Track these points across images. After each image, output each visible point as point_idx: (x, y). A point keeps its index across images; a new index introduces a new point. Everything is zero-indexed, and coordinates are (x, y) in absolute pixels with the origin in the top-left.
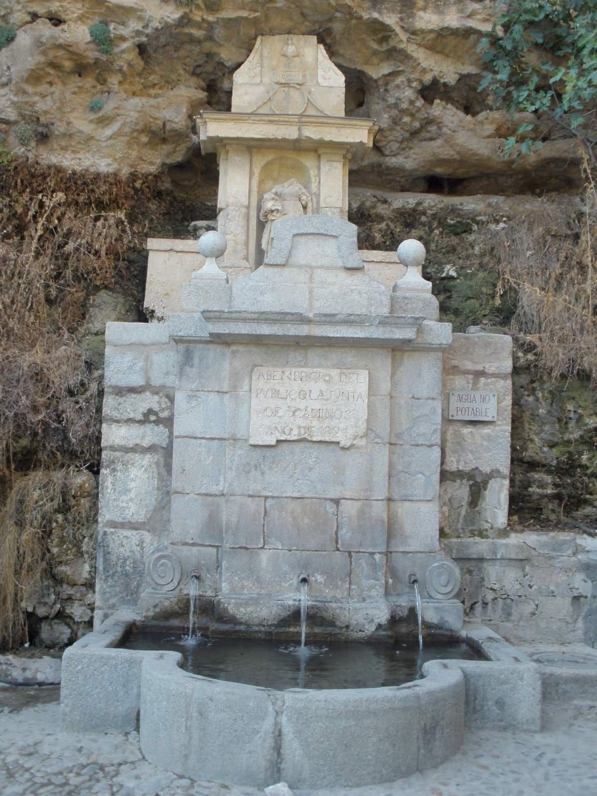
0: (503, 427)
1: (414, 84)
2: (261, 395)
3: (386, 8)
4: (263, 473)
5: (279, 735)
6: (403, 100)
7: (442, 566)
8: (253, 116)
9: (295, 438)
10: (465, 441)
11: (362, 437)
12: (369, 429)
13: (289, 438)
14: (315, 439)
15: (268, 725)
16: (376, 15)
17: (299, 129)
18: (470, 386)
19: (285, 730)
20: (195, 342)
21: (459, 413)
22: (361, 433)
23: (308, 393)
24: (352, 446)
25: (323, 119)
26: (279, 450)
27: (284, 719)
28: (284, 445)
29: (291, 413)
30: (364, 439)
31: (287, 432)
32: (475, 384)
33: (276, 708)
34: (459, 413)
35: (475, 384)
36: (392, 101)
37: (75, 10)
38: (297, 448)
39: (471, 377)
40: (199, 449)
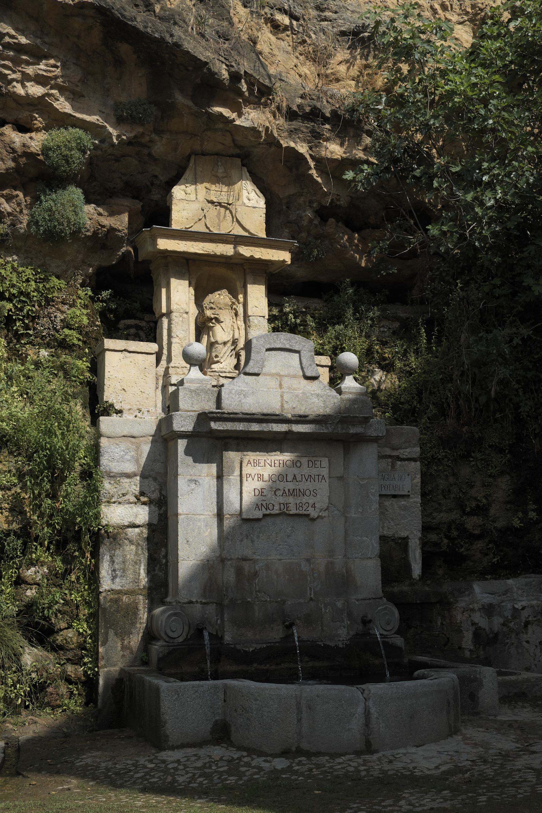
0: (415, 499)
1: (315, 205)
2: (250, 479)
3: (299, 138)
4: (253, 541)
5: (367, 714)
6: (304, 218)
7: (386, 608)
8: (185, 235)
9: (277, 512)
10: (387, 511)
11: (325, 511)
12: (330, 503)
13: (272, 512)
14: (291, 513)
15: (360, 709)
16: (292, 144)
17: (234, 248)
18: (390, 467)
19: (372, 711)
20: (230, 437)
21: (383, 489)
22: (325, 506)
23: (285, 476)
24: (319, 517)
25: (252, 241)
26: (263, 523)
27: (370, 703)
28: (268, 519)
29: (273, 493)
30: (327, 511)
31: (271, 508)
32: (393, 466)
33: (365, 695)
34: (383, 489)
35: (393, 466)
36: (292, 217)
37: (540, 264)
38: (278, 521)
39: (390, 460)
40: (199, 524)
